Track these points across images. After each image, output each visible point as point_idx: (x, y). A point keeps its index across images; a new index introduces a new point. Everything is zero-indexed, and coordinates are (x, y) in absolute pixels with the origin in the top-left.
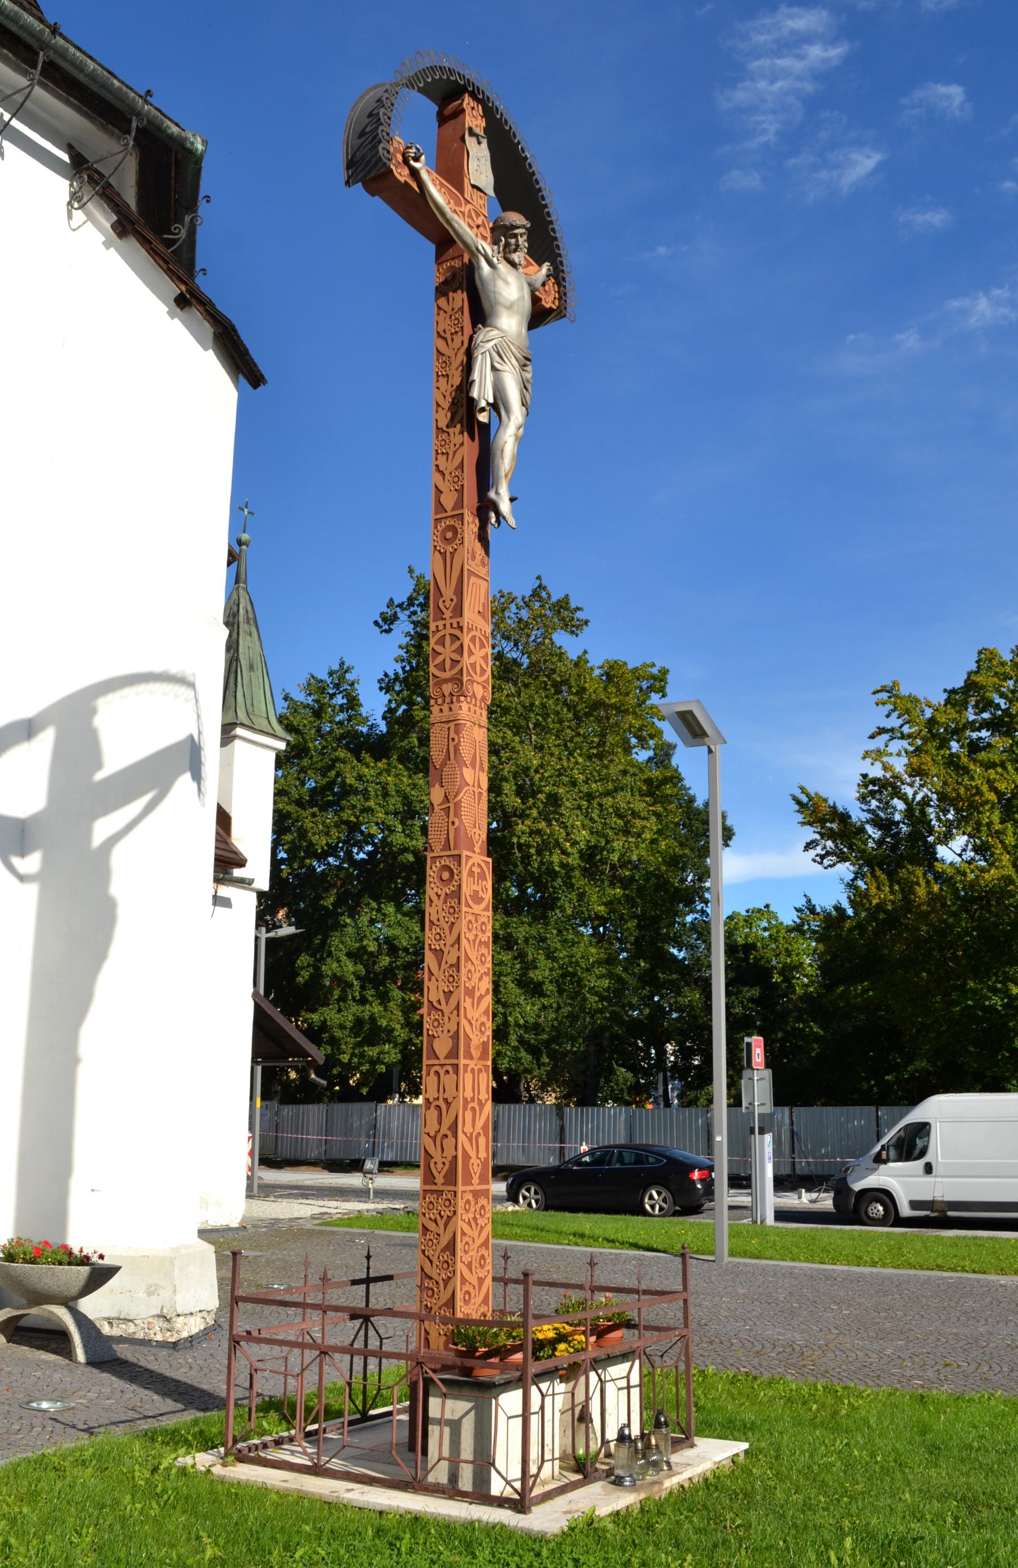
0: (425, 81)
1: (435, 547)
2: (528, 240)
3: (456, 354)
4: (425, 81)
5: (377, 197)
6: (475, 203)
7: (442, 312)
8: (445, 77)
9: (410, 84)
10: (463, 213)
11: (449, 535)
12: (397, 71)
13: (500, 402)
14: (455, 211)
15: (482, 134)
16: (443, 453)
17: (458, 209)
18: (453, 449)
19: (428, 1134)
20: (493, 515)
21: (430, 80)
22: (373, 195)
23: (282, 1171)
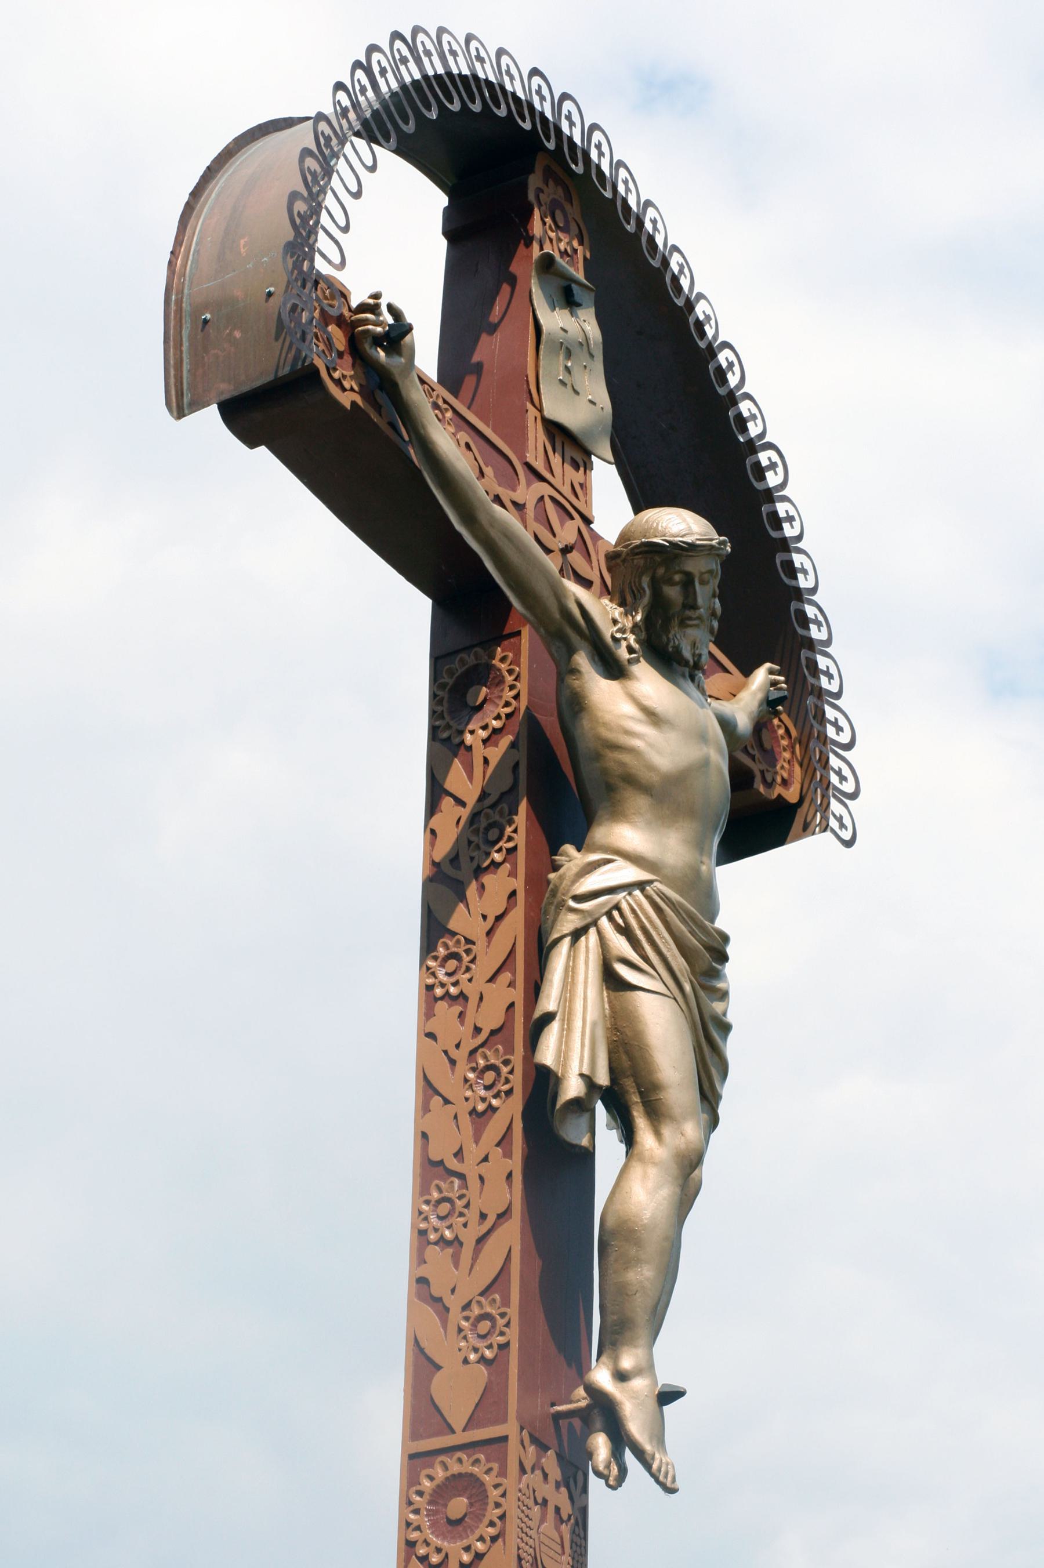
0: (420, 118)
1: (411, 1544)
2: (723, 593)
3: (490, 933)
4: (420, 118)
5: (263, 450)
6: (557, 482)
7: (437, 1100)
8: (477, 107)
9: (374, 129)
10: (519, 507)
11: (458, 1506)
12: (339, 86)
13: (629, 1084)
14: (497, 499)
15: (580, 276)
16: (442, 1241)
17: (506, 495)
18: (476, 1230)
19: (447, 1102)
20: (601, 1445)
21: (456, 107)
22: (252, 444)
23: (426, 423)
